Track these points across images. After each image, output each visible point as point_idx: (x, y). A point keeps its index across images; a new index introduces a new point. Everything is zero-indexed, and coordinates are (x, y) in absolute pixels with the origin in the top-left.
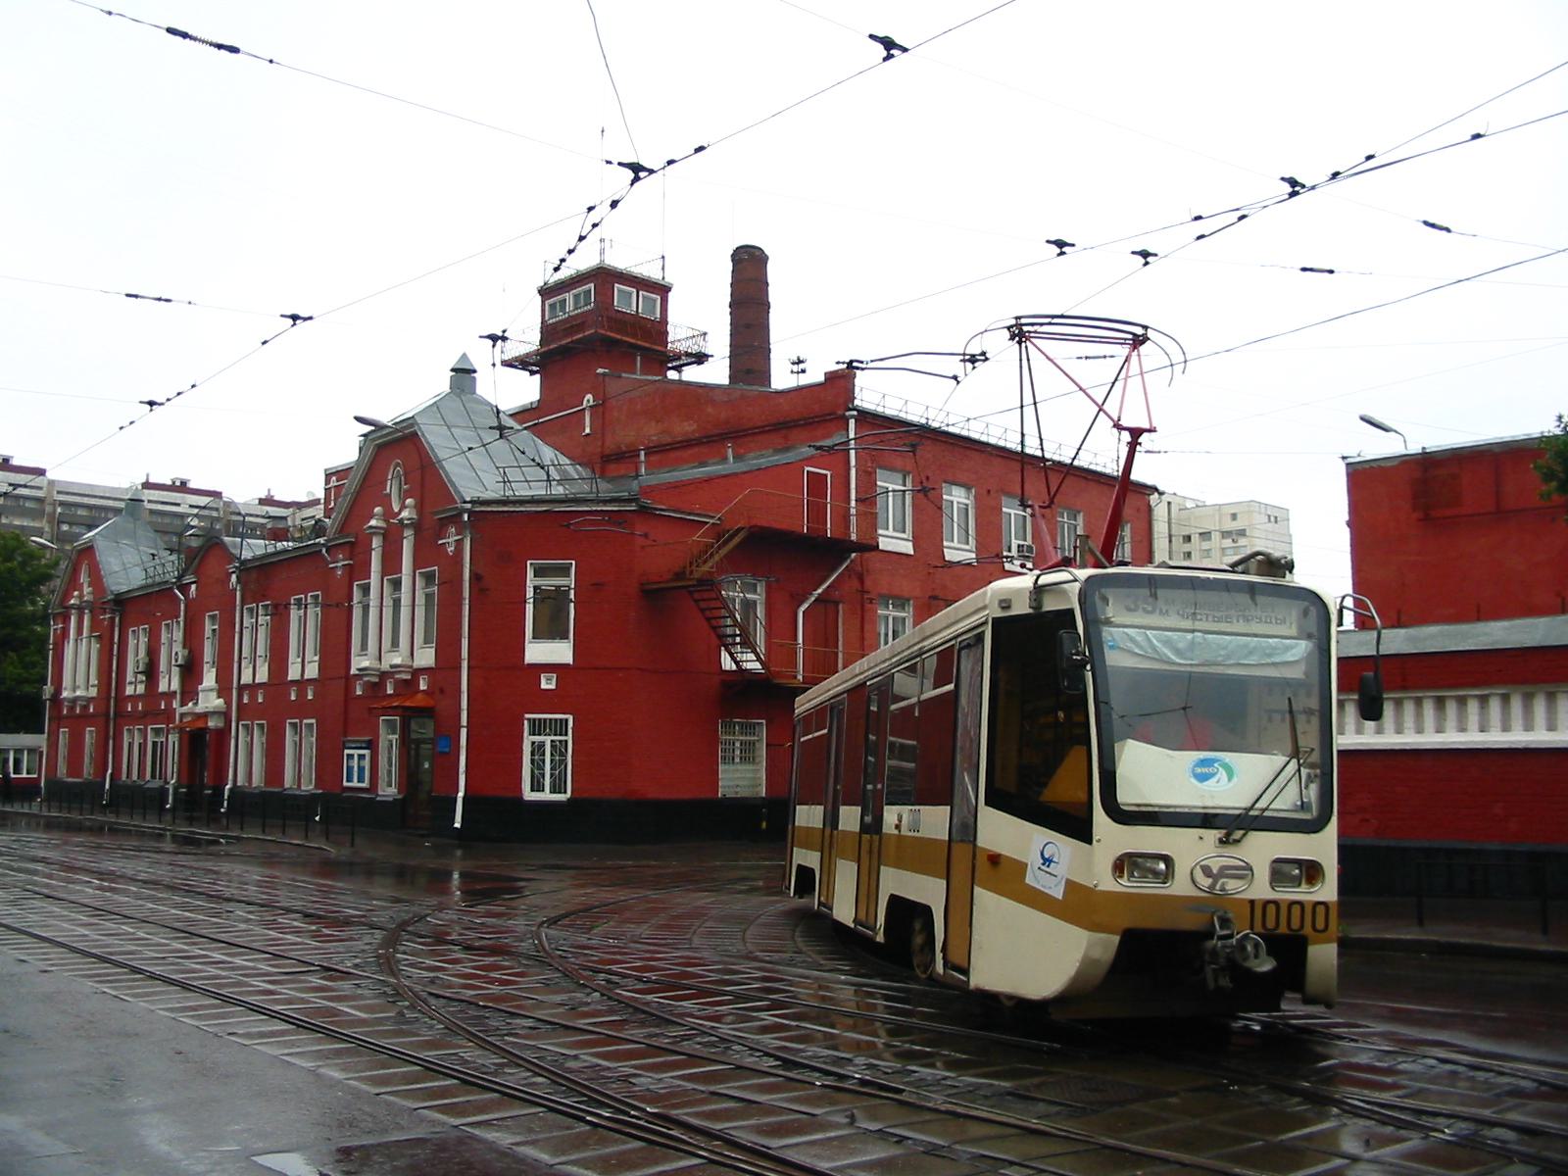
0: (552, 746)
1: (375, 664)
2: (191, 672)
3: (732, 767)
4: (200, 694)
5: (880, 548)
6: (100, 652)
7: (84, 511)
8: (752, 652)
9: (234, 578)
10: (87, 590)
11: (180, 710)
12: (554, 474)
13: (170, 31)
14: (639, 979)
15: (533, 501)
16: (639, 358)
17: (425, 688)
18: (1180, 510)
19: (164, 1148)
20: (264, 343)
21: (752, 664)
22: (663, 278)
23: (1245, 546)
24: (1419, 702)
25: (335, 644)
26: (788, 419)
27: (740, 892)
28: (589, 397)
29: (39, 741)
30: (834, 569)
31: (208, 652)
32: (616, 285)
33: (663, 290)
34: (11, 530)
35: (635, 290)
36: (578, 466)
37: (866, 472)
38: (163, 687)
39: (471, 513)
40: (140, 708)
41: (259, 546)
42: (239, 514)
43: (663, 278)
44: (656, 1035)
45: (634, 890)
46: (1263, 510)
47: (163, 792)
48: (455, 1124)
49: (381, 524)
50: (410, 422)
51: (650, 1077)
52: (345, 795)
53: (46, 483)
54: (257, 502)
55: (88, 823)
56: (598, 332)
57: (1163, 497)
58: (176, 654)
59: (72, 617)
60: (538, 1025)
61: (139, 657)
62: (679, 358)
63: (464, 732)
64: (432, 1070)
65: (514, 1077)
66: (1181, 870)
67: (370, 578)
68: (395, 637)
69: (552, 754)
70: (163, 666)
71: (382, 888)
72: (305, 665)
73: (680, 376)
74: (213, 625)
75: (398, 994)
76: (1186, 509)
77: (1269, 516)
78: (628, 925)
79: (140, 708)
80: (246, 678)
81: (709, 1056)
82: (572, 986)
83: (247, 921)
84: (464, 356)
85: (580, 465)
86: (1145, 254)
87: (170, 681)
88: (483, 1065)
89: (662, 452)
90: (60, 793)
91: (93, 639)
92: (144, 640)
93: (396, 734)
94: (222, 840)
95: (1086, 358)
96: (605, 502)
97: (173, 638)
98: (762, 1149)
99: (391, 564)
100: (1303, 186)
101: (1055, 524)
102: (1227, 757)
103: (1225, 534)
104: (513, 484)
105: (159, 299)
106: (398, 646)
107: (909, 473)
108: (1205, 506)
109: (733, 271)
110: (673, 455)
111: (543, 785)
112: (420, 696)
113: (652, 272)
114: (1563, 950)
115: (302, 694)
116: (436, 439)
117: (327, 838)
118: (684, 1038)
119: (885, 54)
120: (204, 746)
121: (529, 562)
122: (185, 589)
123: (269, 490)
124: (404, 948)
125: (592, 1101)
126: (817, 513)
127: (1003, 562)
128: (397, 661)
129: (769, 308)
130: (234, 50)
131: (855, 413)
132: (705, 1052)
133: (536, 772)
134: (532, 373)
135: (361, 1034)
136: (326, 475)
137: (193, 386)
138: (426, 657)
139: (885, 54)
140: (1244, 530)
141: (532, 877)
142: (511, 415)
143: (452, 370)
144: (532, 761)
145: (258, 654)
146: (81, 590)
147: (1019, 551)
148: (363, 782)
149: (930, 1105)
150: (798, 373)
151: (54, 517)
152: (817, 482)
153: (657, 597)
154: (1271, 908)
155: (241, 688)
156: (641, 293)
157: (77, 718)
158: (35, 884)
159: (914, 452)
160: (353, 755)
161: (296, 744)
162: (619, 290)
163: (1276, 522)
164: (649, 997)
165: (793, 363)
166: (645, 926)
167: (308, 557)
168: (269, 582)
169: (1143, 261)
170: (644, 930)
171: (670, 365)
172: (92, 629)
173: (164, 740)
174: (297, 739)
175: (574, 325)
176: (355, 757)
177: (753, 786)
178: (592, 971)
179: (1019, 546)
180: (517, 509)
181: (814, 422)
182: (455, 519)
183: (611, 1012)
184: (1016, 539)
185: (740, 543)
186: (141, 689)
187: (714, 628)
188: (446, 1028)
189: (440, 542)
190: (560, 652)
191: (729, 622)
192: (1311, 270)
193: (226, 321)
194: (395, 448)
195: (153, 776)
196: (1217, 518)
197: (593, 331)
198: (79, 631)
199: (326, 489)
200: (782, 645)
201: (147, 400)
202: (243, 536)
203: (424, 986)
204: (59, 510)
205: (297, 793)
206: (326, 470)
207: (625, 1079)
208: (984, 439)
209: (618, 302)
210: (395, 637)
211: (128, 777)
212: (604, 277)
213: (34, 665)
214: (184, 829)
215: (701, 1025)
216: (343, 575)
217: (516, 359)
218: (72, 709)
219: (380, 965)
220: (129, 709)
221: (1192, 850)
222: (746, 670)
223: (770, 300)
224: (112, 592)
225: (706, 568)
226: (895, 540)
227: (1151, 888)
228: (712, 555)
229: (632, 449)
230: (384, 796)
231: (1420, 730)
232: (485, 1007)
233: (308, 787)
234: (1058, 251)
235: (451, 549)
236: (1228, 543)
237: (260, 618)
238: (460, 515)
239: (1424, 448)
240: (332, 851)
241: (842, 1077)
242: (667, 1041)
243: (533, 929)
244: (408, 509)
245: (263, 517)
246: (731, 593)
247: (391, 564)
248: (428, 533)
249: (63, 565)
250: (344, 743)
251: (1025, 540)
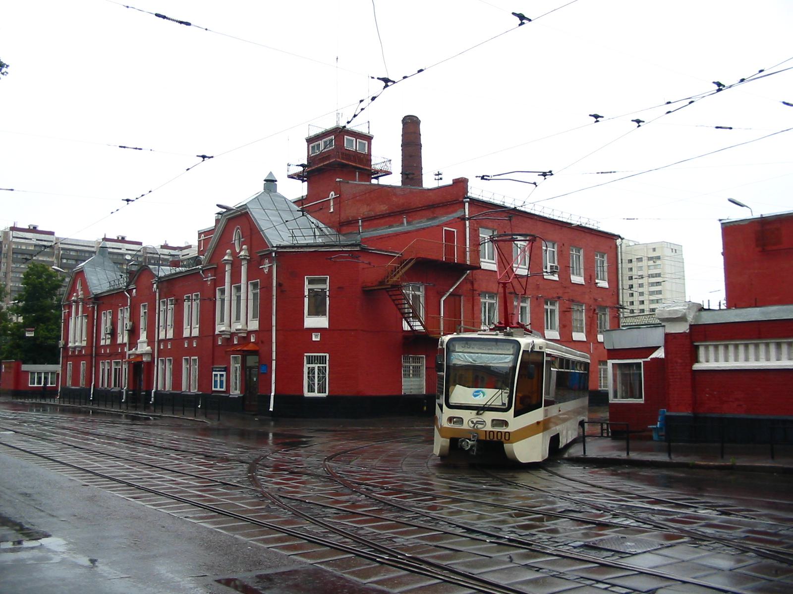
0: (318, 369)
1: (228, 329)
2: (133, 333)
3: (408, 379)
4: (139, 344)
5: (482, 268)
6: (87, 323)
7: (76, 254)
8: (419, 321)
9: (155, 286)
10: (80, 293)
11: (128, 352)
12: (317, 233)
13: (157, 15)
14: (383, 488)
15: (308, 246)
16: (357, 173)
17: (254, 341)
18: (627, 246)
19: (171, 575)
20: (188, 169)
21: (418, 326)
22: (369, 133)
23: (660, 265)
24: (767, 345)
25: (207, 319)
26: (434, 203)
27: (419, 443)
28: (333, 193)
29: (58, 368)
30: (458, 280)
31: (142, 324)
32: (345, 136)
33: (369, 138)
34: (41, 263)
35: (355, 139)
36: (328, 228)
37: (474, 229)
38: (119, 341)
39: (276, 252)
40: (108, 352)
41: (167, 270)
42: (157, 254)
43: (369, 133)
44: (399, 517)
45: (365, 442)
46: (669, 246)
47: (121, 393)
48: (311, 563)
49: (231, 258)
50: (244, 207)
51: (402, 538)
52: (213, 394)
53: (55, 239)
54: (160, 247)
55: (84, 409)
56: (335, 161)
57: (624, 240)
58: (126, 324)
59: (73, 306)
60: (339, 512)
61: (107, 326)
62: (378, 173)
63: (274, 363)
64: (292, 535)
65: (334, 539)
66: (465, 422)
67: (225, 286)
68: (238, 315)
69: (318, 374)
70: (119, 331)
71: (235, 441)
72: (192, 330)
73: (378, 181)
74: (144, 310)
75: (264, 496)
76: (630, 246)
77: (672, 249)
78: (368, 460)
79: (108, 352)
80: (162, 336)
81: (428, 527)
82: (350, 492)
83: (178, 459)
84: (271, 173)
85: (329, 227)
86: (638, 121)
87: (123, 338)
88: (317, 533)
89: (370, 220)
90: (68, 394)
91: (83, 317)
92: (109, 317)
94: (151, 418)
95: (602, 173)
96: (344, 246)
97: (124, 317)
98: (470, 575)
99: (236, 278)
100: (724, 86)
101: (569, 255)
102: (484, 390)
103: (650, 259)
104: (297, 238)
105: (136, 149)
106: (240, 319)
107: (495, 230)
108: (639, 244)
109: (403, 128)
110: (375, 222)
111: (314, 389)
112: (251, 345)
113: (363, 130)
114: (791, 467)
115: (190, 344)
116: (257, 214)
117: (206, 417)
118: (414, 518)
119: (520, 22)
120: (141, 370)
121: (305, 277)
122: (130, 291)
123: (166, 241)
124: (260, 473)
125: (376, 550)
126: (450, 251)
127: (543, 275)
128: (240, 327)
129: (421, 146)
130: (188, 24)
131: (468, 200)
132: (427, 525)
133: (311, 383)
134: (303, 181)
135: (251, 517)
136: (199, 234)
137: (150, 192)
138: (254, 325)
139: (520, 22)
140: (660, 256)
141: (312, 436)
142: (294, 202)
143: (265, 180)
144: (309, 377)
145: (168, 324)
146: (78, 293)
147: (551, 269)
148: (223, 388)
149: (548, 551)
150: (438, 180)
151: (59, 256)
152: (450, 235)
153: (370, 294)
154: (492, 433)
155: (159, 341)
156: (358, 140)
157: (76, 356)
158: (66, 440)
159: (510, 220)
160: (217, 375)
161: (188, 369)
162: (347, 139)
163: (676, 252)
164: (390, 497)
165: (436, 175)
166: (376, 461)
167: (192, 276)
168: (173, 287)
169: (637, 125)
170: (376, 462)
171: (373, 176)
172: (83, 312)
173: (120, 367)
174: (164, 367)
175: (323, 157)
176: (218, 375)
177: (419, 389)
178: (357, 484)
179: (551, 266)
180: (299, 250)
181: (447, 205)
182: (268, 255)
183: (373, 505)
184: (549, 262)
185: (411, 267)
186: (108, 342)
187: (399, 309)
188: (293, 514)
189: (261, 267)
190: (322, 322)
191: (406, 306)
192: (721, 128)
193: (142, 156)
194: (236, 221)
195: (115, 385)
196: (645, 250)
197: (334, 160)
198: (77, 313)
199: (199, 241)
200: (433, 318)
201: (126, 199)
202: (159, 265)
203: (276, 492)
204: (61, 252)
205: (189, 393)
207: (390, 539)
208: (533, 212)
209: (346, 145)
210: (238, 315)
211: (102, 386)
212: (339, 132)
213: (53, 330)
214: (133, 412)
215: (420, 511)
217: (295, 174)
218: (74, 352)
219: (250, 482)
220: (103, 352)
221: (468, 416)
222: (416, 330)
223: (422, 142)
224: (93, 293)
225: (395, 279)
226: (489, 264)
227: (457, 426)
228: (398, 272)
229: (355, 219)
230: (233, 395)
231: (768, 359)
232: (309, 503)
233: (194, 390)
234: (595, 120)
235: (266, 271)
236: (651, 263)
237: (168, 306)
238: (271, 253)
239: (762, 215)
240: (209, 423)
241: (499, 538)
242: (405, 520)
243: (322, 462)
244: (244, 251)
245: (168, 255)
246: (408, 292)
247: (236, 278)
249: (67, 280)
250: (212, 369)
251: (554, 263)
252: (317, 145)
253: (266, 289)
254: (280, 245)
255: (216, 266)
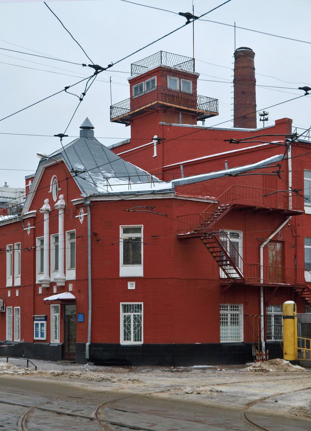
15: (122, 194)
16: (181, 115)
25: (29, 268)
33: (194, 78)
56: (161, 103)
68: (57, 267)
69: (134, 322)
84: (87, 120)
93: (58, 313)
99: (53, 229)
106: (58, 269)
113: (187, 68)
115: (13, 293)
133: (126, 331)
134: (127, 125)
143: (80, 128)
144: (125, 325)
148: (43, 337)
150: (264, 120)
176: (40, 326)
189: (76, 217)
190: (137, 271)
206: (26, 177)
212: (162, 72)
216: (30, 234)
233: (18, 340)
235: (81, 220)
247: (53, 229)
248: (71, 212)
250: (34, 317)
252: (152, 81)
253: (81, 237)
254: (94, 194)
255: (35, 216)
